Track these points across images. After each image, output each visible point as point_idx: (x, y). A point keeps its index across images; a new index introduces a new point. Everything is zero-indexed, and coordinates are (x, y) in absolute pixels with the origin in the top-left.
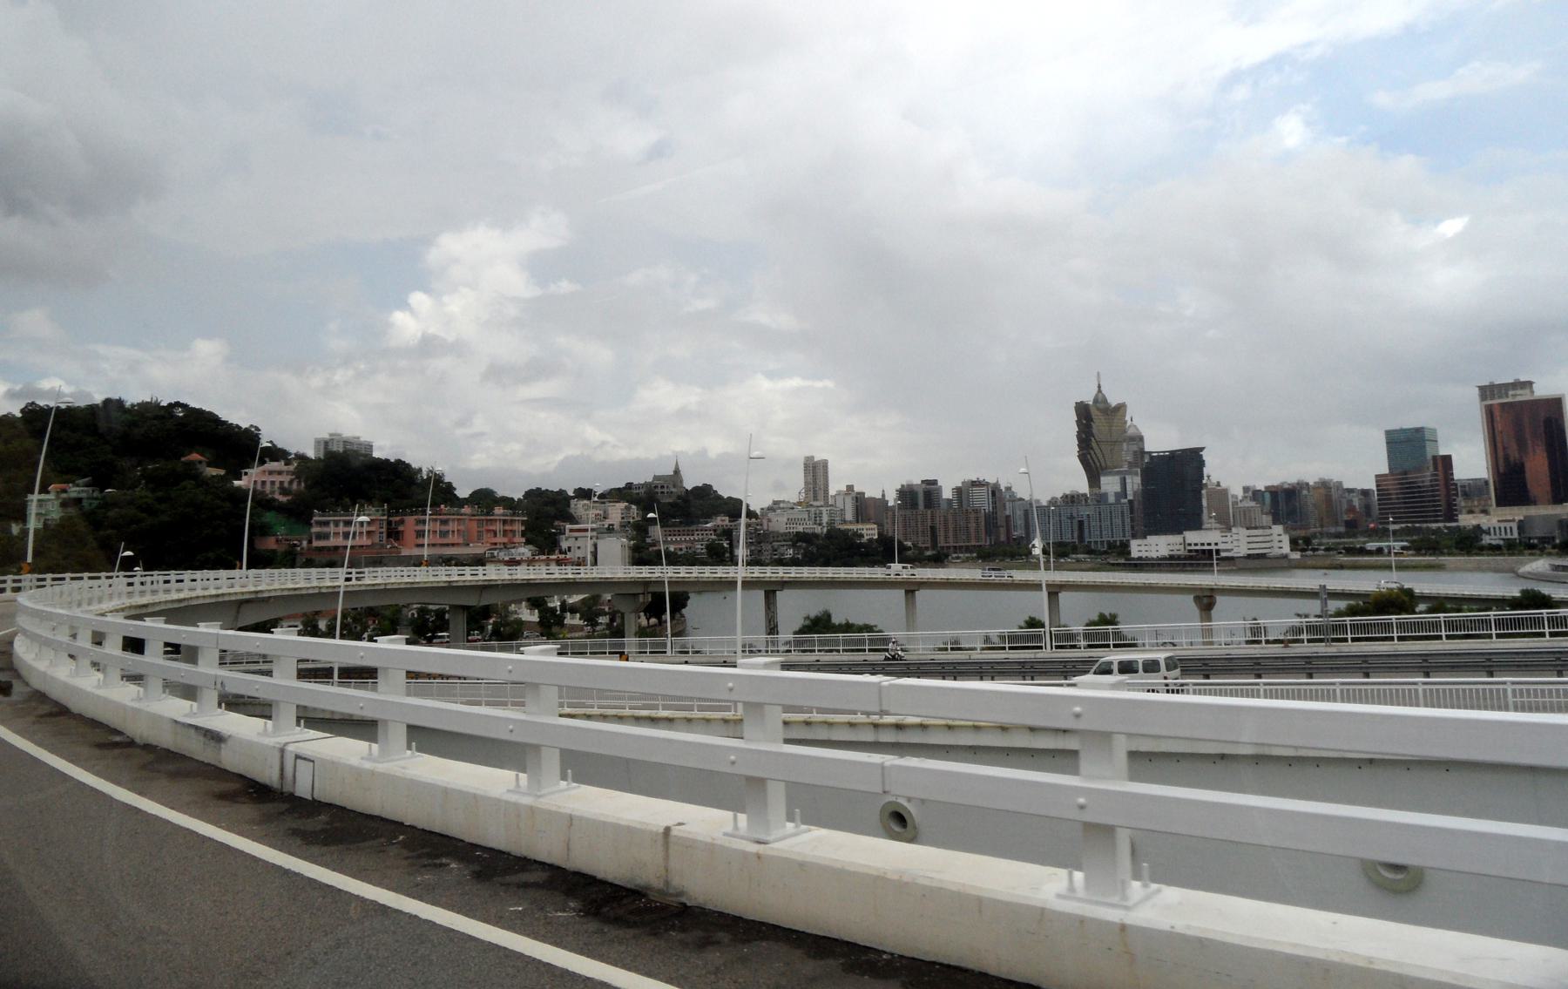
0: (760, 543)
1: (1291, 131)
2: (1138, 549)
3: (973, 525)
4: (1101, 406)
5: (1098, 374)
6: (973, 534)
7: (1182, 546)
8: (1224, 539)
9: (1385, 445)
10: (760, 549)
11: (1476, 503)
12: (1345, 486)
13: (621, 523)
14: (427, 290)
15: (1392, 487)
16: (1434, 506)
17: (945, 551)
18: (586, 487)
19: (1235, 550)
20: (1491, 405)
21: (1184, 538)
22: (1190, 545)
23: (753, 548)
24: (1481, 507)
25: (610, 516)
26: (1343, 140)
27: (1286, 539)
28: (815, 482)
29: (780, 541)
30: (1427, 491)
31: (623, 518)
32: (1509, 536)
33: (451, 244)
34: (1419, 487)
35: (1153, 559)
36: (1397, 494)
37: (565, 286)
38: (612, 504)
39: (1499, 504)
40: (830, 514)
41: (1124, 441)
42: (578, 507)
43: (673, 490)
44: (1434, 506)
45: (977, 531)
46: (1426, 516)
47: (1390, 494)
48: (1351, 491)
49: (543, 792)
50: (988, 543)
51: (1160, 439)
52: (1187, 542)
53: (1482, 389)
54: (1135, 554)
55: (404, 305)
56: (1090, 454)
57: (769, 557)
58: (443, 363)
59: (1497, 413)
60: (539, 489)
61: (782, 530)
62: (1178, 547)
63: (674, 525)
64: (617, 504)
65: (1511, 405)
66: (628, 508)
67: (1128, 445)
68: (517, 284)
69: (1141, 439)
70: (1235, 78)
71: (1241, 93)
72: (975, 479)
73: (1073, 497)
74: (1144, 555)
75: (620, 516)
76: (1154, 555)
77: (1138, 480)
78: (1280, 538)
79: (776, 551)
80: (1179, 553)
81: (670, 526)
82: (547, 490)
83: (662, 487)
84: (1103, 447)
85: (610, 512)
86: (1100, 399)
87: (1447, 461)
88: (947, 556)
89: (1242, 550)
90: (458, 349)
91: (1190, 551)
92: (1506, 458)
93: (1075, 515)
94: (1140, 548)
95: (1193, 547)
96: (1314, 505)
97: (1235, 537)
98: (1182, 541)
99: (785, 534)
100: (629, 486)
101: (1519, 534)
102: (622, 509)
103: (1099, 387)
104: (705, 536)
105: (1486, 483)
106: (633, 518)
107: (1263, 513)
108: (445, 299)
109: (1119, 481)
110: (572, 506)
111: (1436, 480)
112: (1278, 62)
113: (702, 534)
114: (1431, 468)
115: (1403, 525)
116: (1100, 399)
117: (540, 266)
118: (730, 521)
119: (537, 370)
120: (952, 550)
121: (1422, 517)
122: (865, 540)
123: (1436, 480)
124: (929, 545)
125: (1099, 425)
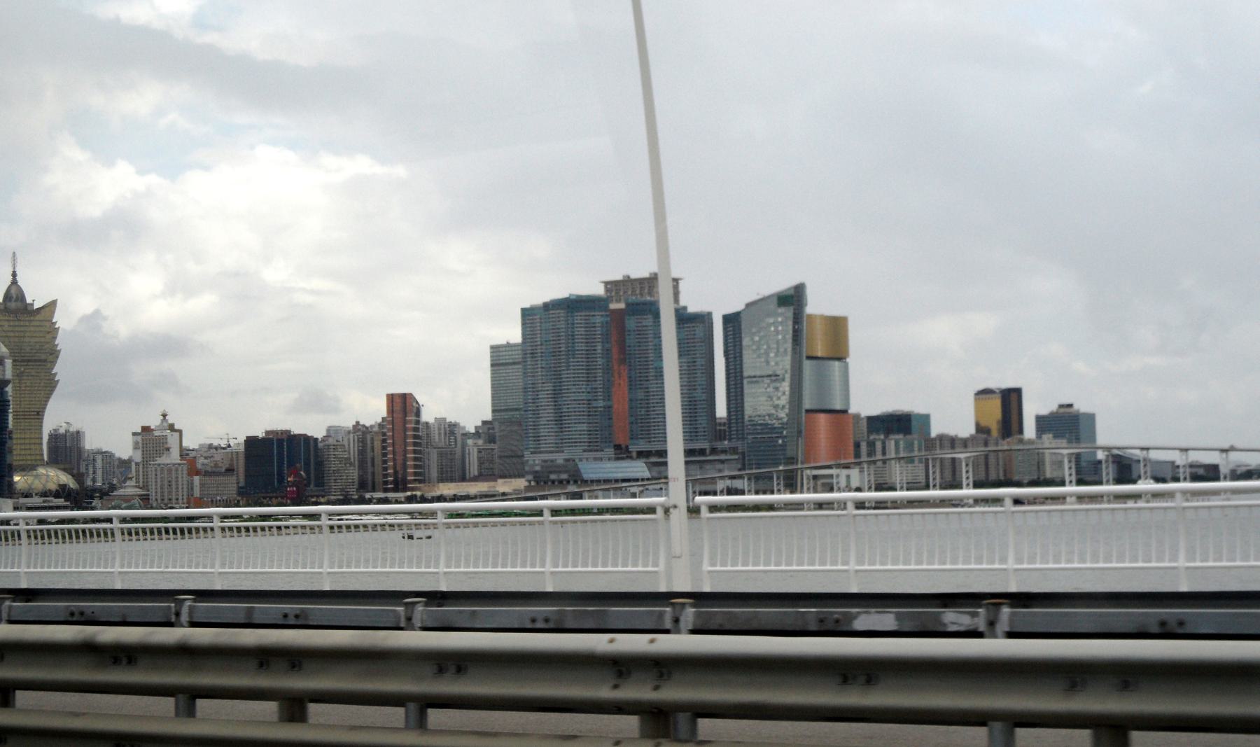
103: (14, 275)
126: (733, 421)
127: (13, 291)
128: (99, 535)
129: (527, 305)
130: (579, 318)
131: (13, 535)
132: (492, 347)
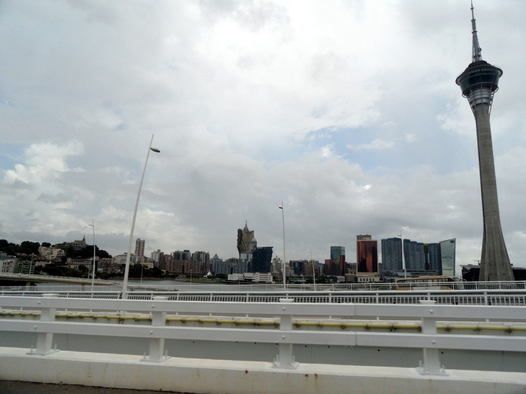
0: (107, 267)
1: (326, 152)
2: (230, 277)
3: (197, 266)
4: (246, 231)
5: (246, 220)
6: (196, 269)
7: (243, 277)
8: (254, 276)
9: (330, 251)
10: (107, 269)
11: (353, 271)
12: (320, 263)
13: (57, 256)
14: (24, 164)
15: (329, 264)
16: (339, 270)
17: (177, 274)
18: (47, 242)
19: (256, 280)
20: (359, 241)
21: (244, 275)
22: (245, 277)
23: (104, 268)
24: (354, 272)
25: (53, 253)
26: (341, 157)
27: (272, 277)
28: (139, 247)
29: (116, 267)
30: (337, 266)
31: (58, 254)
32: (342, 281)
33: (36, 148)
34: (335, 264)
35: (234, 281)
36: (330, 266)
37: (80, 170)
38: (55, 249)
39: (358, 271)
40: (139, 259)
41: (251, 243)
42: (42, 250)
43: (81, 246)
44: (339, 270)
45: (198, 269)
46: (336, 272)
47: (328, 266)
48: (320, 264)
49: (160, 361)
50: (202, 273)
51: (261, 244)
52: (245, 276)
53: (358, 236)
54: (229, 279)
55: (13, 168)
56: (241, 246)
57: (110, 272)
58: (24, 192)
59: (360, 243)
60: (28, 242)
61: (119, 263)
62: (241, 278)
63: (79, 258)
64: (57, 249)
65: (364, 242)
66: (60, 251)
67: (252, 244)
68: (59, 165)
69: (256, 243)
70: (311, 133)
71: (313, 138)
72: (200, 251)
73: (232, 259)
74: (231, 279)
75: (57, 253)
76: (234, 280)
77: (252, 255)
78: (270, 277)
79: (113, 270)
80: (241, 279)
81: (76, 259)
82: (31, 242)
83: (77, 245)
84: (245, 244)
85: (53, 252)
86: (246, 229)
87: (344, 257)
88: (178, 276)
89: (258, 280)
90: (29, 187)
91: (245, 279)
92: (362, 257)
93: (230, 265)
94: (230, 277)
95: (246, 278)
96: (308, 268)
97: (256, 275)
98: (243, 276)
99: (119, 264)
100: (65, 243)
101: (345, 280)
102: (58, 251)
103: (246, 225)
104: (86, 263)
105: (356, 263)
106: (62, 255)
107: (291, 269)
108: (31, 168)
109: (246, 256)
110: (39, 248)
111: (340, 263)
112: (323, 130)
113: (87, 262)
114: (339, 259)
115: (330, 276)
116: (246, 229)
117: (70, 161)
118: (99, 258)
119: (61, 198)
120: (179, 274)
121: (335, 272)
122: (148, 269)
123: (340, 263)
124: (181, 272)
125: (245, 236)
126: (345, 265)
127: (246, 228)
128: (363, 287)
129: (382, 239)
130: (396, 242)
131: (302, 288)
132: (331, 247)
